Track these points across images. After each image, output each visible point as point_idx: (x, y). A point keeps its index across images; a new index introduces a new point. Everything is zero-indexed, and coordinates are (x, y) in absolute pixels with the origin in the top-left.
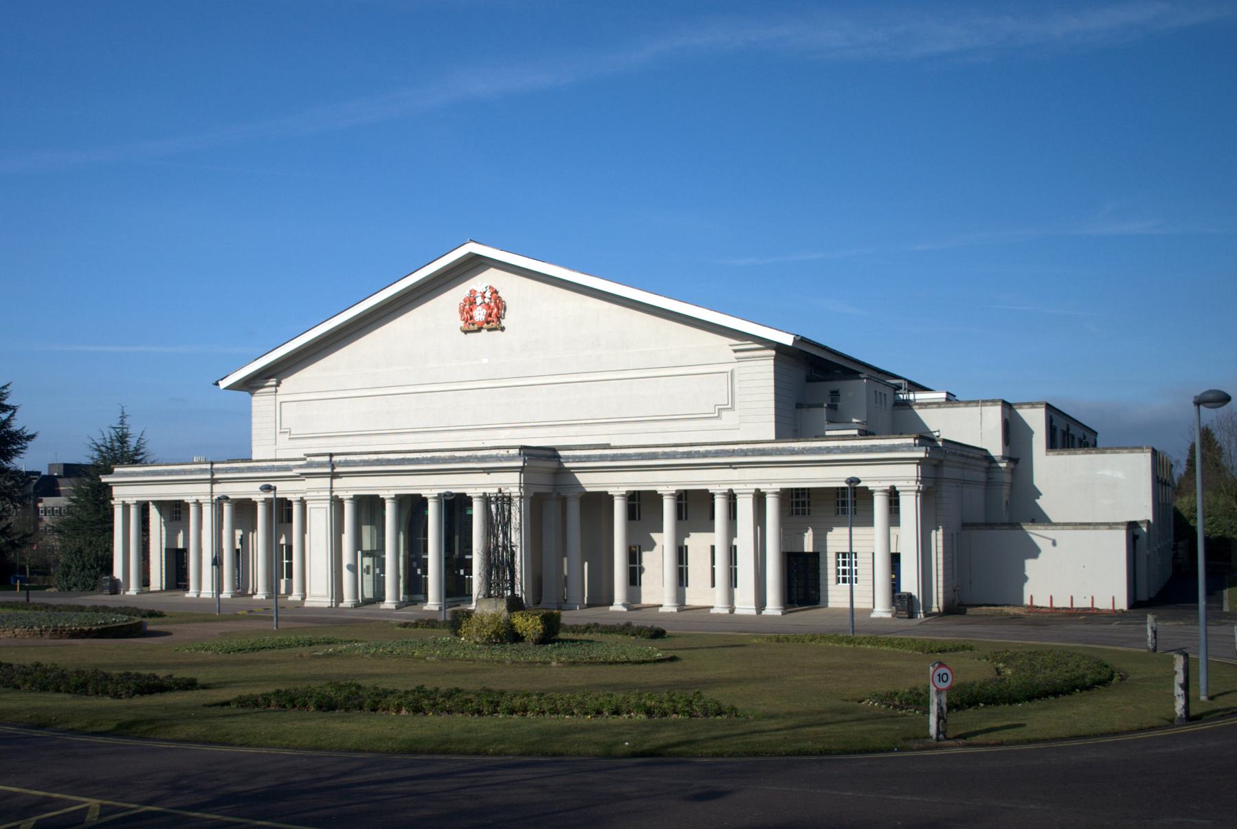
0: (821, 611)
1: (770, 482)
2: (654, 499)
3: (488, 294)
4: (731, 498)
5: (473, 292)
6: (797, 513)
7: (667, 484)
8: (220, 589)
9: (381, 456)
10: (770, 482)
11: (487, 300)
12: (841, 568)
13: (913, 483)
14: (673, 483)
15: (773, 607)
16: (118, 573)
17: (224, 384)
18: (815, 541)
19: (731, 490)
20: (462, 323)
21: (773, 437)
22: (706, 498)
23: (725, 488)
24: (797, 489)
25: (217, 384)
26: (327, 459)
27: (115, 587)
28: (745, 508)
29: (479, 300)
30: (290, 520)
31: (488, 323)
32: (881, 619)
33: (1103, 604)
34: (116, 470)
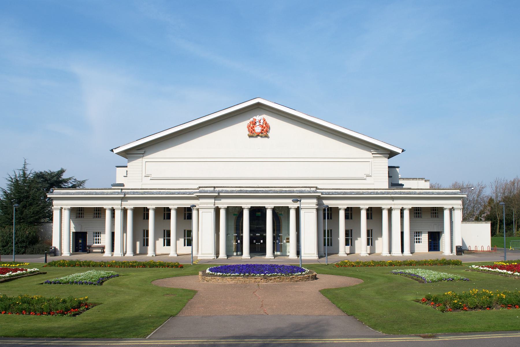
0: (263, 257)
2: (240, 210)
3: (262, 121)
4: (113, 211)
6: (79, 217)
9: (242, 189)
13: (315, 205)
16: (55, 244)
17: (116, 151)
19: (113, 208)
20: (248, 133)
21: (387, 187)
22: (379, 210)
23: (110, 207)
24: (79, 208)
25: (112, 151)
26: (213, 189)
27: (55, 252)
28: (118, 214)
29: (258, 124)
30: (148, 218)
31: (262, 133)
32: (108, 257)
33: (486, 249)
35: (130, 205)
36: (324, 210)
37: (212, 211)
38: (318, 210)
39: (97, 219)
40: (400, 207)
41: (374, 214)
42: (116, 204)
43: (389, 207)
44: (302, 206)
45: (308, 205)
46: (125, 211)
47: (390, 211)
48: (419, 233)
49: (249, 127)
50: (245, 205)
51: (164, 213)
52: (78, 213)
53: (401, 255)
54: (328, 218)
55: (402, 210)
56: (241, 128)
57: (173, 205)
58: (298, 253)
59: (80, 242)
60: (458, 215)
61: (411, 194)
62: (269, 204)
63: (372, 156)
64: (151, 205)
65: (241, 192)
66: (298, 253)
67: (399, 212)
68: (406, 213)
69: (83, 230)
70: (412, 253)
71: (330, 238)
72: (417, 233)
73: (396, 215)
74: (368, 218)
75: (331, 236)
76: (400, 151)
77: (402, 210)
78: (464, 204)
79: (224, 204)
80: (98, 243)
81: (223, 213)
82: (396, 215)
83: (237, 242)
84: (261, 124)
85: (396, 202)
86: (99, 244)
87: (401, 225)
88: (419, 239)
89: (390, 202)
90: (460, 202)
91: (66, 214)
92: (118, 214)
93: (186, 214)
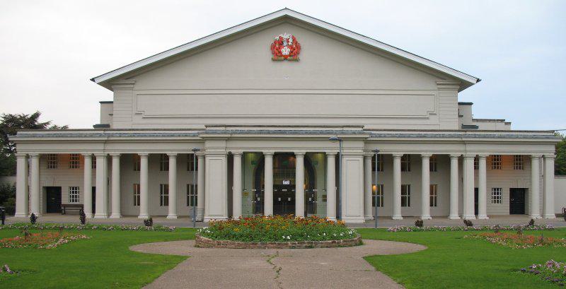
1: (483, 151)
2: (261, 158)
3: (291, 40)
4: (94, 158)
5: (281, 38)
6: (51, 167)
7: (426, 151)
8: (109, 214)
10: (115, 150)
11: (290, 43)
12: (72, 194)
14: (240, 148)
15: (116, 214)
18: (286, 185)
23: (90, 153)
28: (101, 163)
29: (285, 44)
30: (167, 169)
32: (115, 219)
34: (18, 133)
35: (117, 150)
36: (373, 158)
37: (224, 160)
38: (365, 158)
39: (75, 170)
40: (474, 154)
41: (441, 163)
42: (98, 150)
43: (459, 154)
44: (344, 152)
45: (351, 151)
46: (109, 159)
47: (94, 158)
48: (498, 189)
49: (273, 47)
50: (454, 153)
51: (159, 162)
52: (50, 161)
53: (335, 220)
54: (378, 170)
55: (477, 159)
56: (262, 48)
57: (172, 150)
58: (338, 216)
59: (52, 200)
60: (550, 165)
61: (488, 137)
62: (300, 149)
63: (436, 87)
64: (143, 150)
65: (261, 132)
66: (338, 216)
67: (472, 162)
68: (483, 164)
69: (57, 185)
70: (542, 216)
71: (137, 195)
72: (495, 189)
73: (469, 164)
74: (431, 169)
75: (135, 197)
76: (475, 82)
77: (477, 159)
78: (557, 148)
79: (238, 148)
80: (76, 201)
81: (237, 162)
82: (469, 164)
83: (256, 199)
84: (290, 43)
85: (469, 147)
86: (77, 203)
87: (475, 179)
88: (498, 197)
89: (461, 147)
90: (553, 148)
91: (35, 163)
92: (101, 163)
93: (188, 163)
